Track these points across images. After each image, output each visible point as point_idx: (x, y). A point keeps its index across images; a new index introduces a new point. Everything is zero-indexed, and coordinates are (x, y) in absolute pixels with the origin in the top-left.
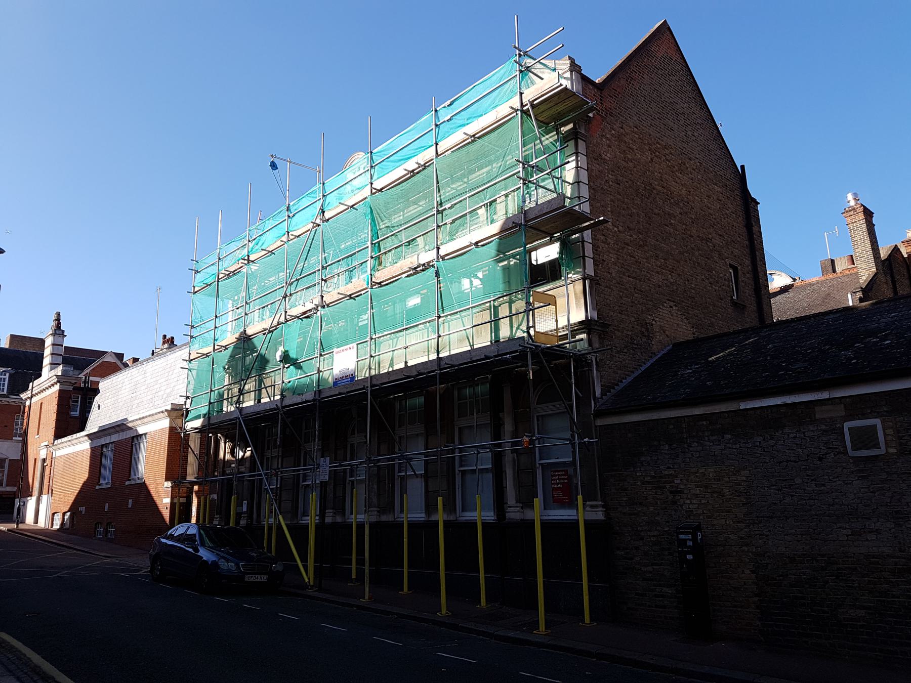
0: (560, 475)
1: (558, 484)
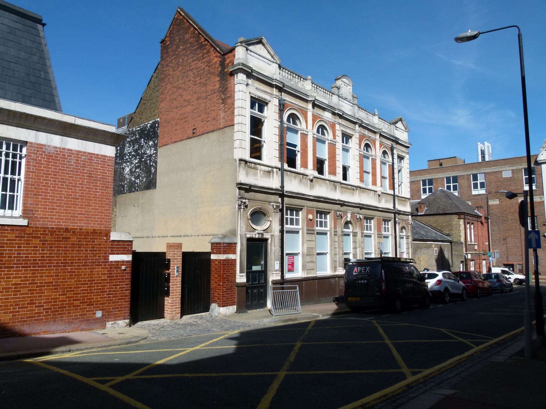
0: (291, 258)
1: (290, 262)
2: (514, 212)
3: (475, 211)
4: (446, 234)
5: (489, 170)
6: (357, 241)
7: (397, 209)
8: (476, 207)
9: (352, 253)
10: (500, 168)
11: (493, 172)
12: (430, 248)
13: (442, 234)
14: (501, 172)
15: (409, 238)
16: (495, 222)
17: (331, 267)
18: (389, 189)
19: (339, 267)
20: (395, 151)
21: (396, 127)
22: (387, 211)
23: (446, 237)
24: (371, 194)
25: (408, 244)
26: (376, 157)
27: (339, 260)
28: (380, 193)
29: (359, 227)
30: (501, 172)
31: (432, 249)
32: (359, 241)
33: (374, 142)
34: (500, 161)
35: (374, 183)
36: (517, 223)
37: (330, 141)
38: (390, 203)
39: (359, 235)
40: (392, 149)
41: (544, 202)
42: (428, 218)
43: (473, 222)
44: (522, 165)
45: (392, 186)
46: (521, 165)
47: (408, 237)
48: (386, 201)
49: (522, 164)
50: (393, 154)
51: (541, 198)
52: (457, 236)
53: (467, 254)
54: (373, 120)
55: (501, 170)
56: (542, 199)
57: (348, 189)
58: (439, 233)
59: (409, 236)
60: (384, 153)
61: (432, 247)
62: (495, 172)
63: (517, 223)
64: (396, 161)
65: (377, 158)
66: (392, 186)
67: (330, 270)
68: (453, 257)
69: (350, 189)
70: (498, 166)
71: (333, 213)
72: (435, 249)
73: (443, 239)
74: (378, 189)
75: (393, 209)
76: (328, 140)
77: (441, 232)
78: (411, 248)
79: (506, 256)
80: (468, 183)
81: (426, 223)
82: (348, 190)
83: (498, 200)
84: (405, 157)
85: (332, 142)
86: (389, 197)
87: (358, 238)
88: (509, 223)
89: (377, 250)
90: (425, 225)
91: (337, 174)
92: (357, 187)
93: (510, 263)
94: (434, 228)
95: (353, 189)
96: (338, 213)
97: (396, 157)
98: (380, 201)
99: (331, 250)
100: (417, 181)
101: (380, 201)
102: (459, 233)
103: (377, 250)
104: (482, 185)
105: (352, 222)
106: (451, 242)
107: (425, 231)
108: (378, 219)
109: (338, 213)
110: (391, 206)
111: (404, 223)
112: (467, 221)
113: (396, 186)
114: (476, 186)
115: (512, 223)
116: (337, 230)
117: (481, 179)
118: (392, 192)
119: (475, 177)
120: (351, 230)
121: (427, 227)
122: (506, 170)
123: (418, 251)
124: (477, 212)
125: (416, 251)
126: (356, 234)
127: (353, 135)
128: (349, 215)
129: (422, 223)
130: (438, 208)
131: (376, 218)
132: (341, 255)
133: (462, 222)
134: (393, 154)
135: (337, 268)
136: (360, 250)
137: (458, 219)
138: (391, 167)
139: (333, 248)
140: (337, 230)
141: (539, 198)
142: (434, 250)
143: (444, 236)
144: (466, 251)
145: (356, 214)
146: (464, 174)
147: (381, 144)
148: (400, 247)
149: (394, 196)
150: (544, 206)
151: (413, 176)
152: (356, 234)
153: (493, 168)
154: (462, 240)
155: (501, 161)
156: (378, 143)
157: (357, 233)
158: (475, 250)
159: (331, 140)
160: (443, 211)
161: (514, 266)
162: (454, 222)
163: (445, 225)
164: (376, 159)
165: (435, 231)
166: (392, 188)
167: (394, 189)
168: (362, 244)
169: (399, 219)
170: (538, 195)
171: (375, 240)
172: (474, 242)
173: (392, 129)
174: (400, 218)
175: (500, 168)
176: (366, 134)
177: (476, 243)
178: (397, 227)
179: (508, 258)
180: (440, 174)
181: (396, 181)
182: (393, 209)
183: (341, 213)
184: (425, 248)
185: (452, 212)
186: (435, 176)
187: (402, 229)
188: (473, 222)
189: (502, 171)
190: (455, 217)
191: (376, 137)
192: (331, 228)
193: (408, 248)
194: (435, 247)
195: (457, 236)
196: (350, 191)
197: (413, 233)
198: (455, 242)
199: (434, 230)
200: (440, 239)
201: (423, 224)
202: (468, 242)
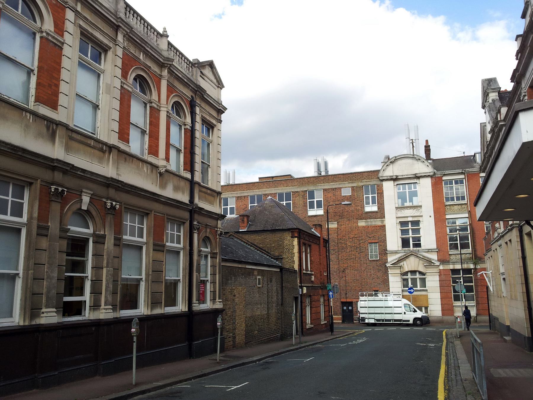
2: (354, 237)
3: (313, 230)
4: (274, 256)
5: (327, 186)
6: (105, 254)
7: (197, 205)
8: (313, 225)
9: (90, 278)
10: (339, 184)
11: (331, 189)
12: (250, 276)
13: (270, 257)
14: (340, 189)
15: (216, 258)
16: (332, 250)
17: (24, 308)
18: (184, 170)
19: (47, 307)
20: (198, 110)
21: (201, 72)
22: (176, 204)
23: (275, 261)
24: (145, 169)
25: (213, 266)
26: (160, 107)
27: (48, 292)
28: (163, 170)
29: (110, 227)
30: (340, 189)
31: (254, 277)
32: (108, 255)
33: (158, 79)
34: (339, 176)
35: (154, 150)
36: (357, 251)
37: (44, 34)
38: (183, 193)
39: (110, 242)
40: (192, 106)
41: (385, 226)
42: (252, 237)
43: (310, 243)
44: (363, 182)
45: (190, 166)
46: (362, 182)
47: (215, 256)
48: (176, 189)
49: (363, 181)
50: (193, 114)
51: (383, 221)
52: (290, 261)
53: (301, 287)
54: (158, 42)
55: (341, 186)
56: (383, 222)
57: (89, 146)
58: (265, 256)
59: (216, 253)
60: (177, 106)
61: (253, 275)
62: (333, 189)
63: (357, 251)
64: (198, 126)
65: (162, 109)
66: (190, 166)
67: (20, 315)
68: (284, 292)
69: (93, 147)
70: (337, 182)
71: (38, 186)
72: (258, 277)
73: (270, 263)
74: (160, 162)
75: (188, 202)
76: (42, 32)
77: (268, 253)
78: (219, 273)
79: (345, 292)
80: (303, 201)
81: (249, 242)
82: (89, 149)
83: (336, 222)
84: (215, 125)
85: (50, 38)
86: (182, 183)
87: (106, 247)
88: (348, 251)
89: (150, 273)
90: (247, 244)
91: (59, 107)
92: (111, 148)
93: (348, 300)
94: (260, 249)
95: (102, 149)
96: (53, 188)
97: (198, 119)
98: (163, 186)
99: (26, 269)
100: (244, 197)
101: (163, 186)
102: (293, 257)
103: (150, 273)
104: (319, 205)
105: (94, 213)
106: (281, 269)
107: (246, 252)
108: (155, 217)
109: (53, 188)
110: (185, 198)
111: (208, 230)
112: (302, 241)
113: (198, 167)
114: (312, 206)
115: (351, 251)
116: (49, 224)
117: (319, 196)
118: (188, 176)
119: (312, 195)
120: (91, 231)
121: (249, 247)
122: (346, 187)
123: (231, 279)
124: (315, 231)
125: (228, 280)
126: (101, 240)
127: (110, 48)
128: (86, 199)
129: (243, 241)
130: (266, 222)
131: (152, 216)
132: (54, 281)
133: (296, 241)
134: (193, 114)
135: (44, 310)
136: (107, 272)
137: (292, 237)
138: (189, 134)
139: (32, 262)
140: (49, 224)
141: (380, 222)
142: (256, 279)
143: (272, 260)
144: (301, 283)
145: (104, 200)
146: (298, 190)
147: (171, 89)
148: (198, 271)
149: (192, 183)
150: (385, 231)
151: (240, 191)
152: (101, 240)
153: (331, 184)
154: (296, 267)
155: (341, 175)
156: (164, 84)
157: (104, 237)
158: (312, 281)
159: (48, 34)
160: (272, 226)
161: (353, 304)
162: (286, 242)
163: (273, 246)
164: (160, 111)
165: (260, 253)
166: (189, 168)
167: (192, 171)
168: (116, 260)
169: (198, 222)
170: (379, 218)
171: (149, 255)
172: (311, 271)
173: (195, 73)
174: (201, 222)
175: (339, 184)
176: (141, 57)
177: (313, 273)
178: (196, 236)
179: (346, 294)
180: (271, 189)
181: (198, 159)
182: (188, 202)
183: (60, 189)
184: (242, 275)
185: (284, 228)
186: (265, 191)
187: (204, 240)
188: (310, 243)
189: (341, 188)
190: (288, 236)
191: (161, 72)
192: (30, 218)
193: (213, 274)
194: (258, 275)
195: (290, 261)
196: (93, 151)
197: (223, 251)
198: (287, 268)
199: (258, 252)
200: (265, 263)
201: (245, 242)
202: (304, 270)
